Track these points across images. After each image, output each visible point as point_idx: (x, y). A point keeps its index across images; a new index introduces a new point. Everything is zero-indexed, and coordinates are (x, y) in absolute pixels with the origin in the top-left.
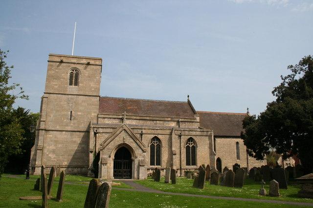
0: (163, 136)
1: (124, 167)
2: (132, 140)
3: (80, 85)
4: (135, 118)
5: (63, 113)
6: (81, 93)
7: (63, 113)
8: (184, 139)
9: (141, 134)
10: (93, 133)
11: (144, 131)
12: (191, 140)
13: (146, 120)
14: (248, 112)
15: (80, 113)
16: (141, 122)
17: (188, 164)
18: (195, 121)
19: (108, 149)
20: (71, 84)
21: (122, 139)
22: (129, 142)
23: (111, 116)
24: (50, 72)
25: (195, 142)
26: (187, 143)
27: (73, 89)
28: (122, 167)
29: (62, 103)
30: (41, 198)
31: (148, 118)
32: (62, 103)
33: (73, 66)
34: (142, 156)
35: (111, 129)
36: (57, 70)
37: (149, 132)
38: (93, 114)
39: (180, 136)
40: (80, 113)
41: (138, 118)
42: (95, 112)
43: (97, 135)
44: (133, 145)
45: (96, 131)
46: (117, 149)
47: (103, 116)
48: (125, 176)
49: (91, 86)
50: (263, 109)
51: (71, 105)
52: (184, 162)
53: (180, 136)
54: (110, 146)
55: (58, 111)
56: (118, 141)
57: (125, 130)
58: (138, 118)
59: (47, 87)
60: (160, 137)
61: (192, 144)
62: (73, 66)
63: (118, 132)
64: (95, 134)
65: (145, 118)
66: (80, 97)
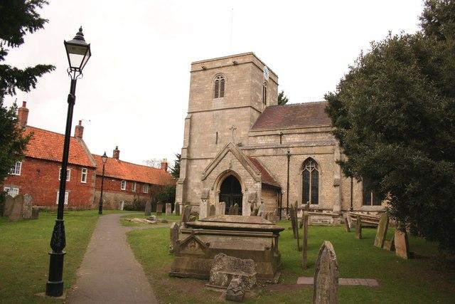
0: (322, 156)
3: (226, 95)
4: (298, 131)
5: (207, 135)
6: (228, 106)
7: (207, 135)
9: (289, 156)
11: (292, 151)
16: (308, 137)
19: (210, 179)
20: (216, 96)
24: (193, 85)
25: (314, 162)
27: (219, 103)
29: (206, 123)
30: (291, 226)
31: (319, 130)
32: (206, 123)
33: (217, 71)
34: (251, 187)
36: (200, 82)
37: (299, 151)
38: (242, 133)
41: (303, 131)
42: (245, 130)
49: (240, 93)
50: (24, 69)
51: (216, 124)
52: (358, 199)
55: (202, 134)
56: (223, 167)
58: (303, 131)
59: (190, 105)
60: (316, 158)
62: (217, 71)
65: (314, 130)
66: (227, 111)
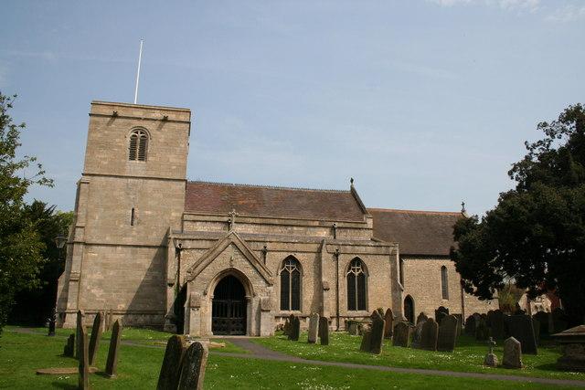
0: (306, 254)
1: (232, 313)
2: (247, 263)
3: (150, 158)
4: (252, 220)
5: (117, 212)
6: (152, 174)
7: (117, 212)
8: (344, 260)
9: (264, 252)
10: (174, 250)
11: (269, 246)
12: (356, 262)
13: (273, 225)
14: (463, 211)
15: (150, 213)
16: (264, 229)
17: (351, 307)
18: (365, 226)
19: (202, 279)
20: (132, 157)
21: (228, 261)
22: (242, 266)
23: (207, 218)
24: (93, 135)
25: (364, 267)
26: (349, 269)
27: (137, 167)
28: (229, 314)
29: (115, 193)
30: (77, 371)
31: (276, 222)
32: (115, 193)
33: (137, 123)
34: (265, 293)
35: (208, 242)
36: (106, 132)
37: (279, 247)
38: (173, 214)
39: (336, 255)
40: (150, 213)
41: (258, 221)
42: (177, 211)
43: (182, 253)
44: (249, 272)
45: (180, 245)
46: (219, 279)
47: (192, 217)
48: (233, 330)
49: (171, 160)
50: (492, 204)
51: (132, 197)
52: (344, 304)
53: (336, 255)
54: (205, 274)
55: (108, 208)
56: (221, 264)
57: (233, 243)
58: (258, 221)
59: (87, 163)
60: (298, 256)
61: (358, 270)
62: (137, 123)
63: (221, 248)
64: (178, 251)
65: (272, 221)
66: (150, 181)
